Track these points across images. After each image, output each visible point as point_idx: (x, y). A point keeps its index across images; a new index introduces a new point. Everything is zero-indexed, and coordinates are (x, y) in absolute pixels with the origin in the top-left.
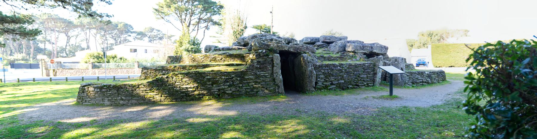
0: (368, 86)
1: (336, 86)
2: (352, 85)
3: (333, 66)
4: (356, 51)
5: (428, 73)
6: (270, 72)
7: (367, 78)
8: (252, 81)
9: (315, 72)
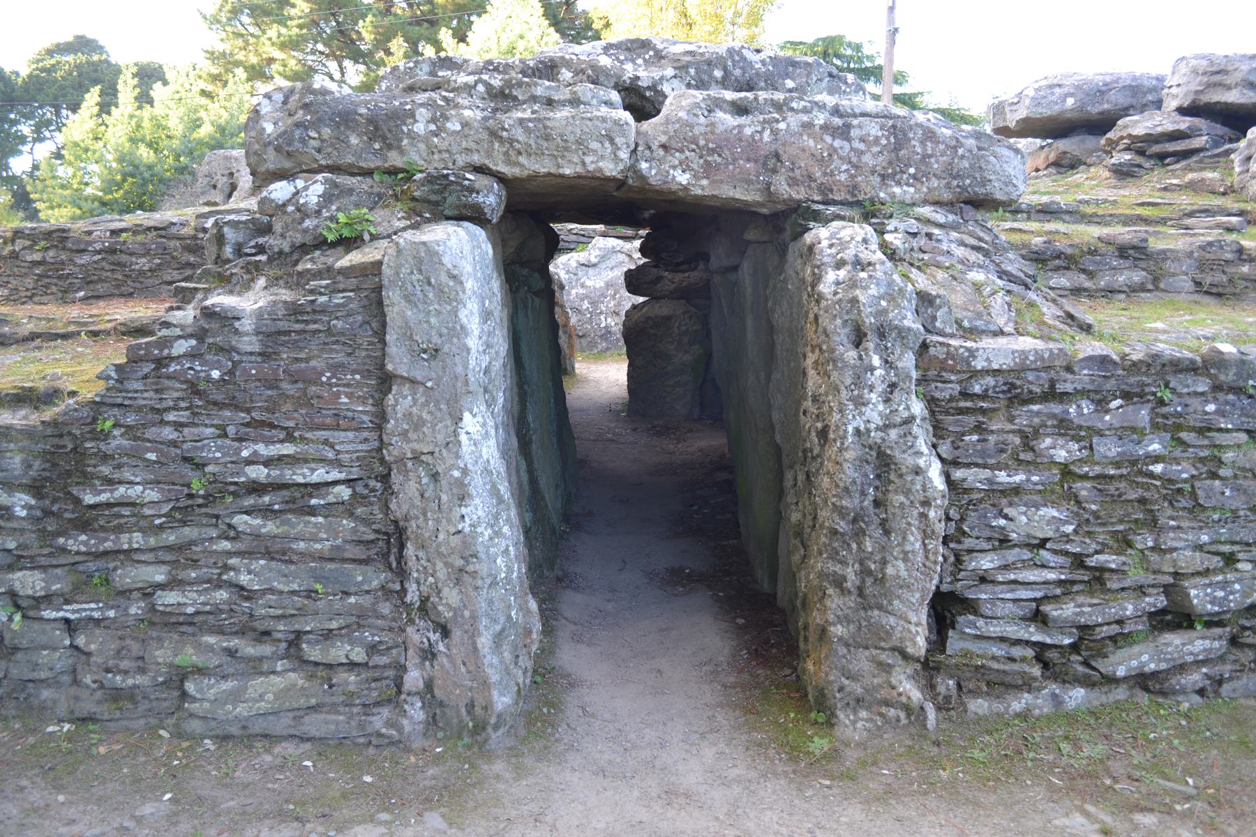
1: (1234, 641)
3: (1217, 388)
6: (349, 443)
8: (137, 539)
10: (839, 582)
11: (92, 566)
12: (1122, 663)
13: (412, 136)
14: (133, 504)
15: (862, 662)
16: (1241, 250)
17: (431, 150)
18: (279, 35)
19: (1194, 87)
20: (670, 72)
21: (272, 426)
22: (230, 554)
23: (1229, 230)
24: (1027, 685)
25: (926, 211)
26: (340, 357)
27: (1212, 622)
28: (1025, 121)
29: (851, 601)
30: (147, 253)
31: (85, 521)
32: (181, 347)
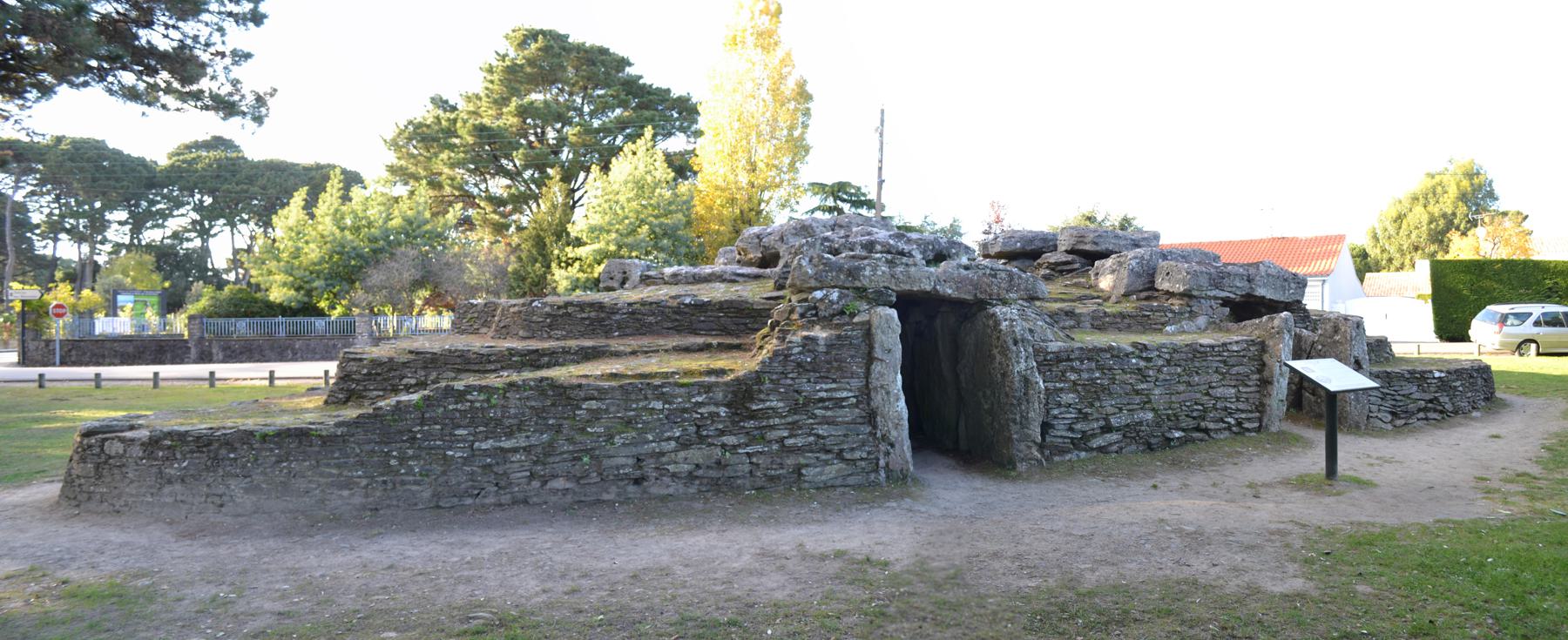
0: (1240, 430)
1: (1124, 436)
2: (1183, 430)
3: (1112, 356)
4: (1195, 293)
5: (1443, 375)
6: (856, 383)
7: (1238, 400)
8: (777, 421)
9: (1041, 383)
10: (1014, 421)
11: (755, 433)
12: (1096, 443)
13: (863, 275)
14: (772, 409)
15: (1022, 446)
16: (1105, 313)
17: (871, 281)
18: (449, 158)
19: (1072, 242)
20: (915, 246)
21: (827, 378)
22: (812, 424)
23: (1099, 304)
24: (1069, 451)
25: (1020, 302)
26: (852, 353)
27: (1118, 429)
28: (1000, 252)
29: (1018, 426)
30: (654, 314)
31: (753, 415)
32: (796, 350)
